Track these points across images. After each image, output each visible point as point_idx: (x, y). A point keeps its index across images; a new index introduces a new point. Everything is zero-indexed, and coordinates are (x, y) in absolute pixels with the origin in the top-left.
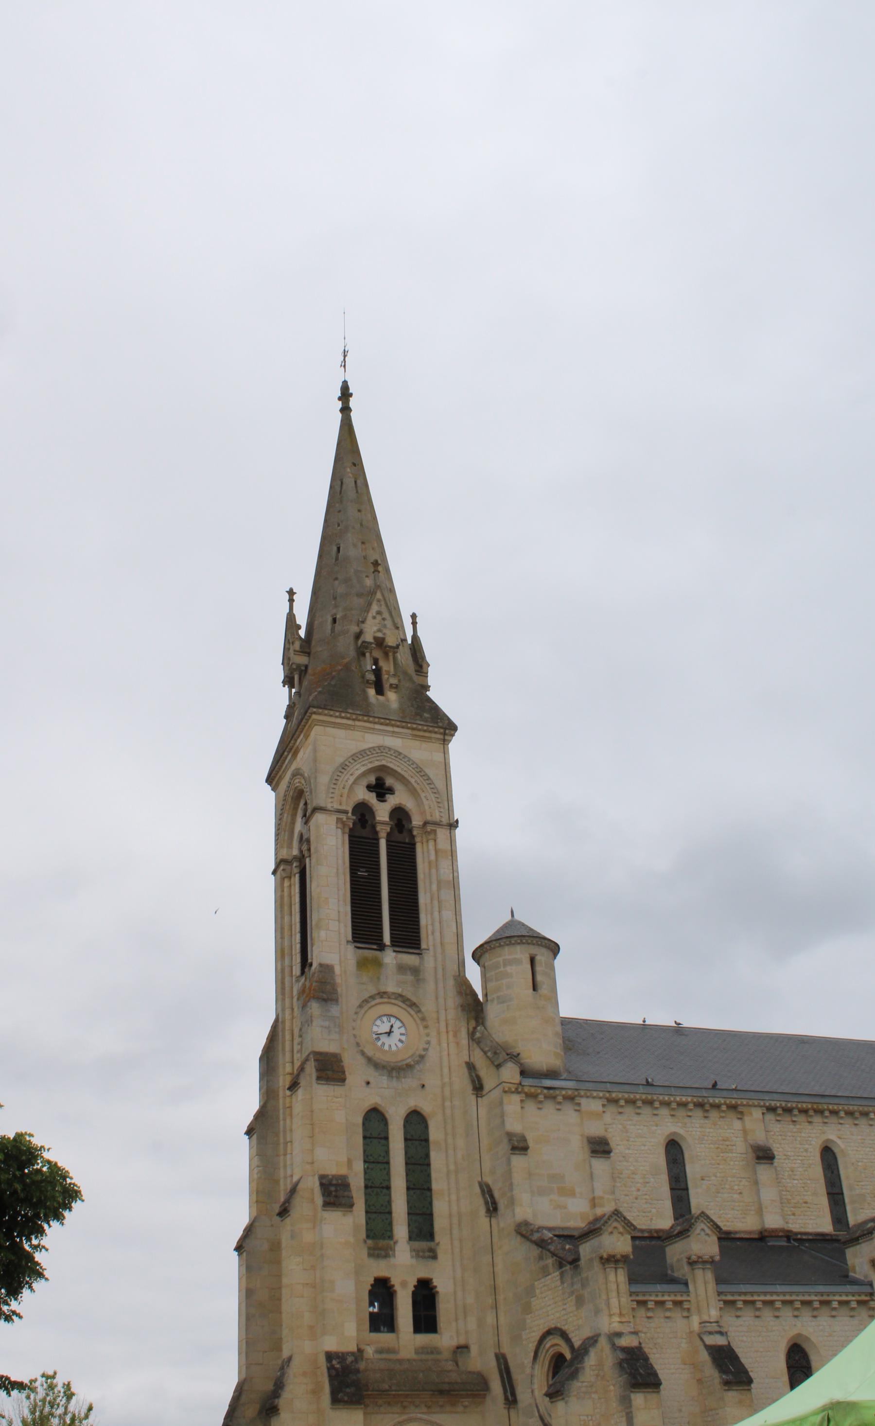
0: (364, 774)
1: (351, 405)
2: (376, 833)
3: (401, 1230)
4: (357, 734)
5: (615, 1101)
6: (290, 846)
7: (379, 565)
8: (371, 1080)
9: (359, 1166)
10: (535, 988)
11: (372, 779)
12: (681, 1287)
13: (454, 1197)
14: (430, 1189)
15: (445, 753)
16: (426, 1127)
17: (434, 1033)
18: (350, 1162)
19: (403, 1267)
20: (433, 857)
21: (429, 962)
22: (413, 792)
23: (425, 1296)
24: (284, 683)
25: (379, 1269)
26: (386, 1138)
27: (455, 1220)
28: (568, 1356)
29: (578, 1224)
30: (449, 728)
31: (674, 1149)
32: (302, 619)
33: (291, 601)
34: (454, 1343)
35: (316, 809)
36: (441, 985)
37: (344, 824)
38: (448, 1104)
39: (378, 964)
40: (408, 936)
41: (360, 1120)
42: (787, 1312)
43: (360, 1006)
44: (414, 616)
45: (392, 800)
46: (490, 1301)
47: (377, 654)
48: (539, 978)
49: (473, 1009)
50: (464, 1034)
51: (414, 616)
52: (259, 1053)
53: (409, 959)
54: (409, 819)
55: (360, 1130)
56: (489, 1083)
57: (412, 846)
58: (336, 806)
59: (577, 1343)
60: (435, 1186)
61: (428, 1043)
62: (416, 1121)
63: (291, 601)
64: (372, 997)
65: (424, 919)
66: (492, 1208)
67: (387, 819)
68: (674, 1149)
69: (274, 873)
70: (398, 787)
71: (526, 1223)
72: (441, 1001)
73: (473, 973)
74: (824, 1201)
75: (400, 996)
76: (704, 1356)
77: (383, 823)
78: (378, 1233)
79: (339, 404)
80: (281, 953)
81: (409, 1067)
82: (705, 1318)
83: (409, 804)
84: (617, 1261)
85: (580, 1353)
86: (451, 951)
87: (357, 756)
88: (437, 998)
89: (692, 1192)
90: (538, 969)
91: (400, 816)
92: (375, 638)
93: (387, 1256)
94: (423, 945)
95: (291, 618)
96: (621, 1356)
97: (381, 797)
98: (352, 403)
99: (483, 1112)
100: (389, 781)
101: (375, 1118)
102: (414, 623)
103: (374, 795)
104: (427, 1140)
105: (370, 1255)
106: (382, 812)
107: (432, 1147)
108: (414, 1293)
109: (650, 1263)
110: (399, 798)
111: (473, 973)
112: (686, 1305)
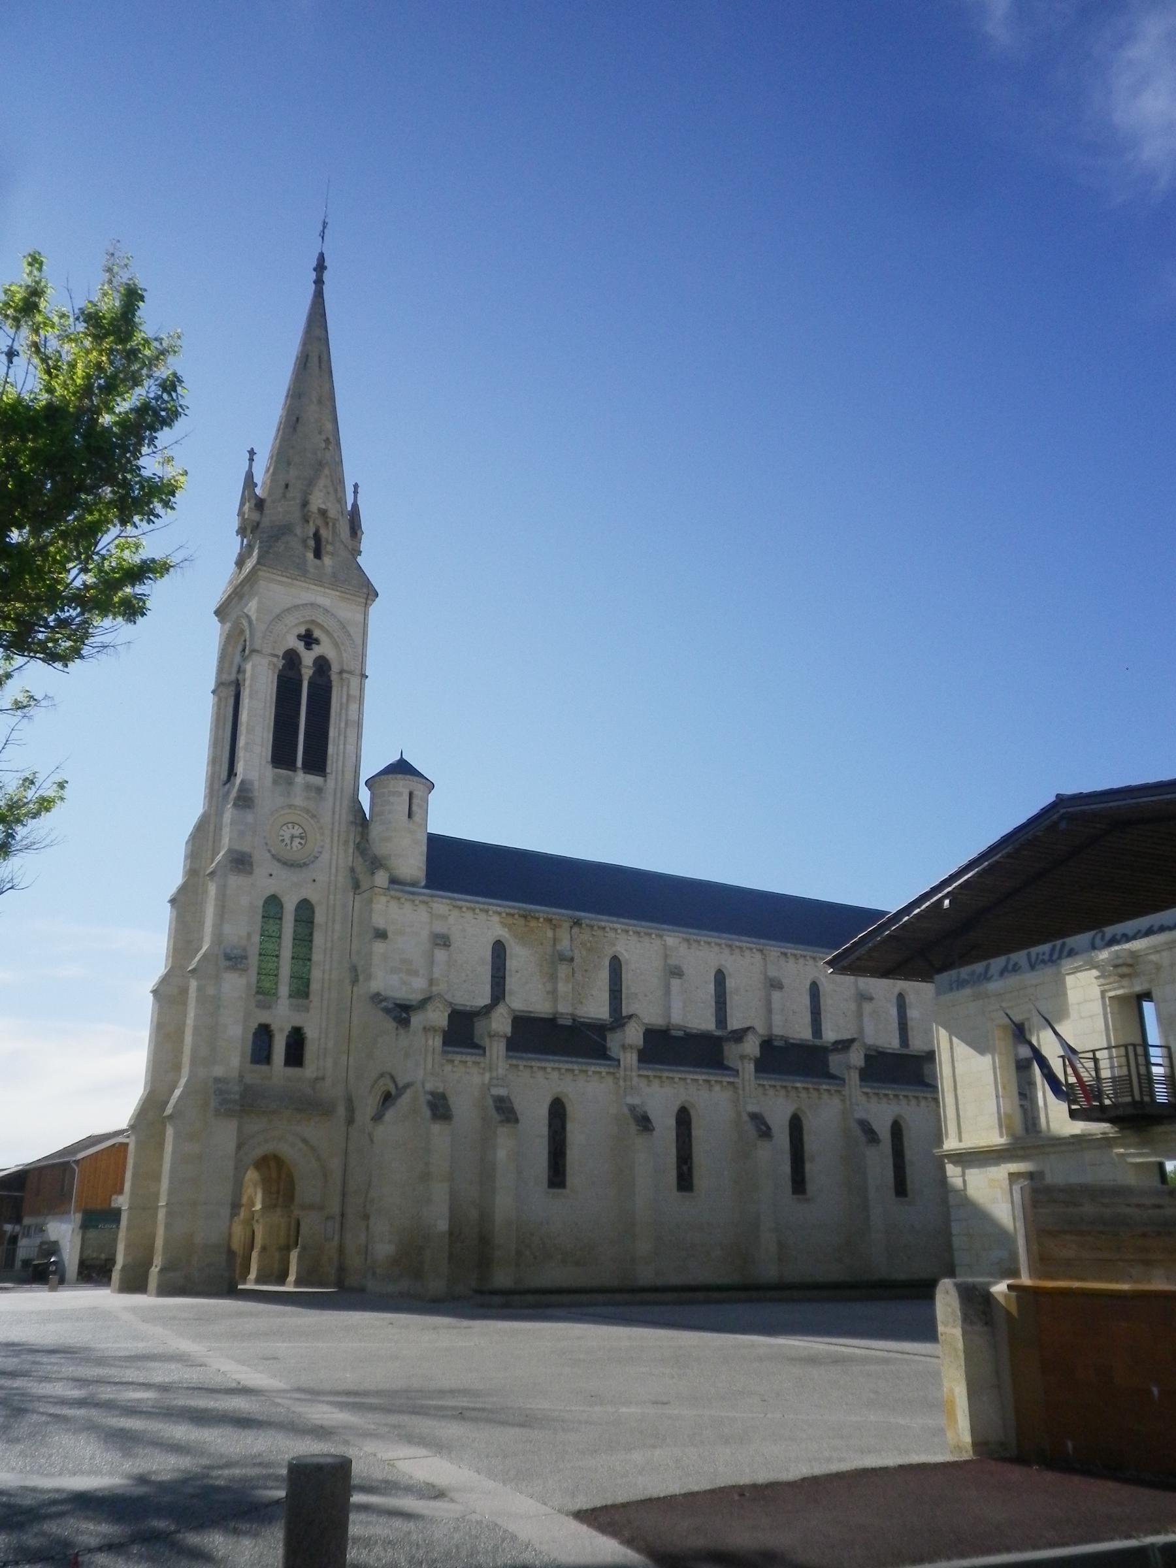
1: (325, 278)
2: (300, 675)
3: (284, 990)
7: (333, 441)
8: (274, 873)
9: (256, 938)
10: (410, 816)
11: (302, 631)
12: (481, 1052)
13: (327, 967)
15: (366, 614)
16: (313, 912)
17: (328, 841)
18: (249, 935)
20: (344, 700)
21: (331, 783)
22: (336, 645)
24: (238, 533)
25: (264, 1017)
27: (326, 985)
28: (393, 1092)
29: (415, 997)
30: (370, 594)
33: (251, 460)
34: (315, 1075)
35: (253, 651)
36: (338, 803)
37: (275, 665)
38: (332, 897)
39: (290, 783)
40: (317, 763)
41: (261, 903)
44: (356, 486)
45: (317, 650)
47: (319, 522)
48: (414, 808)
49: (361, 822)
51: (356, 486)
52: (190, 829)
53: (316, 780)
54: (329, 668)
55: (260, 911)
56: (365, 885)
61: (322, 847)
62: (305, 910)
63: (251, 460)
66: (355, 981)
67: (311, 664)
68: (499, 951)
69: (213, 692)
71: (378, 994)
72: (337, 817)
73: (365, 797)
74: (607, 995)
76: (490, 1102)
77: (307, 667)
78: (264, 994)
79: (313, 275)
80: (214, 761)
81: (305, 864)
82: (494, 1074)
84: (435, 1031)
85: (401, 1091)
86: (349, 776)
88: (334, 813)
89: (508, 980)
90: (415, 801)
91: (322, 665)
92: (319, 509)
93: (269, 1007)
94: (328, 770)
95: (249, 476)
96: (429, 1097)
98: (327, 276)
100: (317, 633)
101: (273, 905)
102: (356, 492)
103: (302, 643)
104: (312, 923)
105: (257, 1006)
106: (308, 658)
108: (288, 1037)
109: (462, 1031)
110: (325, 648)
111: (365, 797)
112: (483, 1065)
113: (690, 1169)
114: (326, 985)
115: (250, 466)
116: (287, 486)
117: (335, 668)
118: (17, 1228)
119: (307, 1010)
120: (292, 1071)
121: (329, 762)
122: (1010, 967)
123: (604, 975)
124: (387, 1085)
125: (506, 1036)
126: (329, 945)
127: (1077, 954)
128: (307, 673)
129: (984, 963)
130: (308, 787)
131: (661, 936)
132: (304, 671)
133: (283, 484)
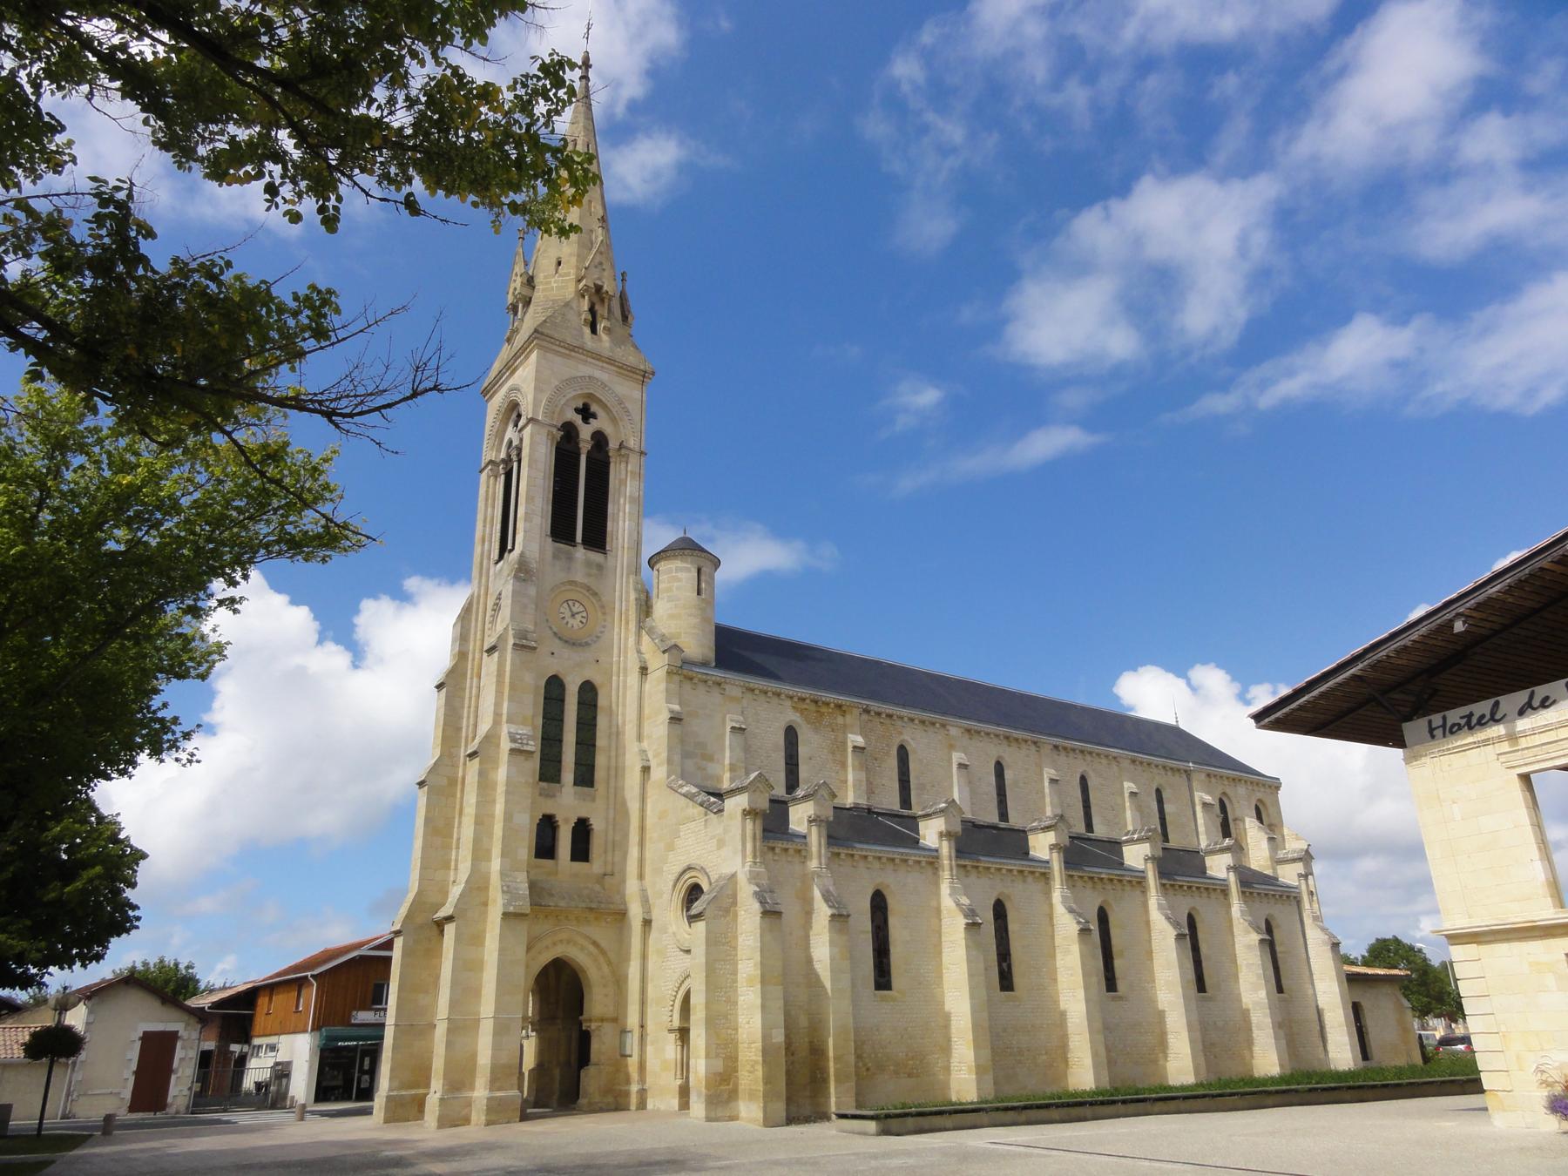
0: (574, 398)
3: (568, 775)
6: (499, 451)
19: (568, 804)
22: (614, 420)
23: (582, 831)
26: (563, 701)
31: (791, 735)
34: (602, 871)
39: (570, 558)
45: (595, 425)
53: (595, 556)
62: (589, 692)
68: (791, 735)
74: (897, 785)
83: (608, 430)
87: (569, 381)
91: (600, 439)
97: (586, 420)
100: (594, 408)
104: (595, 706)
106: (585, 432)
110: (601, 423)
113: (1009, 966)
114: (613, 773)
118: (246, 1048)
119: (593, 800)
120: (579, 866)
122: (1536, 703)
123: (893, 762)
127: (1554, 702)
128: (585, 444)
129: (1491, 702)
130: (588, 564)
131: (943, 726)
132: (581, 445)
133: (554, 262)
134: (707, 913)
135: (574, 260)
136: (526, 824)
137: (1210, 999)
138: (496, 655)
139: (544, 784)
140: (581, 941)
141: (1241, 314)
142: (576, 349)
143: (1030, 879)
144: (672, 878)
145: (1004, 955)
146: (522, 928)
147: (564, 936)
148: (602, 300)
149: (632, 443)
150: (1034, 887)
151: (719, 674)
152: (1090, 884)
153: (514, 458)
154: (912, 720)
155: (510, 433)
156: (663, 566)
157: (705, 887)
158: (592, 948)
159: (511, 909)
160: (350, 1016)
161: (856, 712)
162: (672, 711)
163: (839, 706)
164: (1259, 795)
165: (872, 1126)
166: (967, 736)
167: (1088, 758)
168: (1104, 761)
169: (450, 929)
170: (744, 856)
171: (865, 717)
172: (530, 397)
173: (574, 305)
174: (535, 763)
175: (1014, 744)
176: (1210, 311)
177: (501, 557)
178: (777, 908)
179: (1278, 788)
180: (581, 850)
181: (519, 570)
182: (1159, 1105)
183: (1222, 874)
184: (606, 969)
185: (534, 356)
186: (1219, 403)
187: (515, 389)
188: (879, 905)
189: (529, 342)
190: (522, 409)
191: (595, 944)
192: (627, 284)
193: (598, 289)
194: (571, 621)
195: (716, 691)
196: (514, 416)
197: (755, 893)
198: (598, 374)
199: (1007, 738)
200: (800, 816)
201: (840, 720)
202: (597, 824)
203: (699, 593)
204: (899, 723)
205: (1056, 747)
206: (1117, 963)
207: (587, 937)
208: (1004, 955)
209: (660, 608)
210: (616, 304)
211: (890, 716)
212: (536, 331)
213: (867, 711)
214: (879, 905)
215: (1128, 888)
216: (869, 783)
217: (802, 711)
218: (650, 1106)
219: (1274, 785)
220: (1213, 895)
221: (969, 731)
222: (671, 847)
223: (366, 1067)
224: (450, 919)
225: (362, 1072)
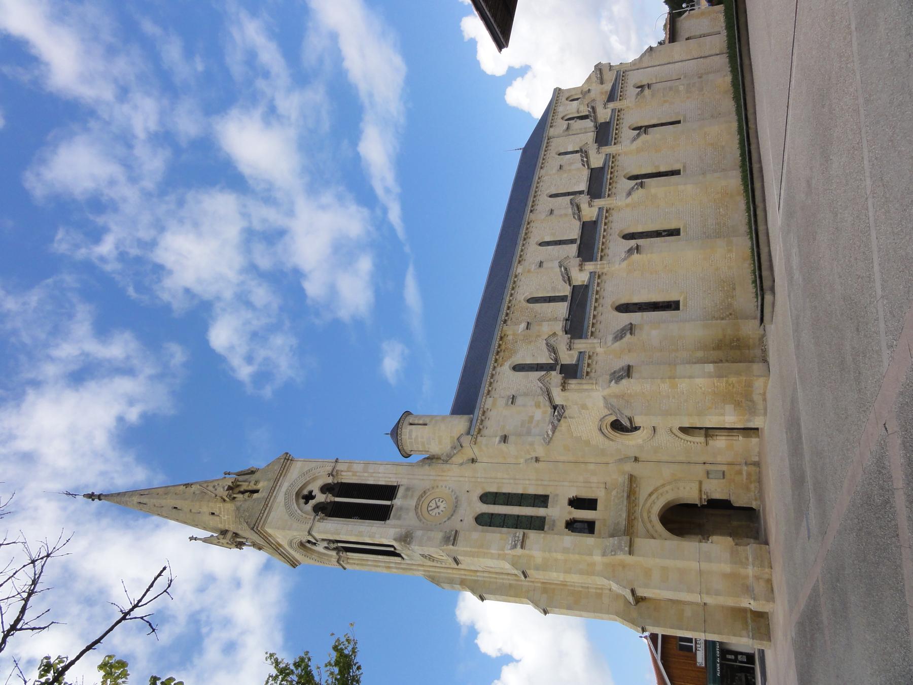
0: (298, 504)
2: (331, 502)
3: (540, 512)
4: (275, 505)
5: (489, 391)
6: (331, 556)
11: (302, 501)
13: (527, 482)
14: (522, 494)
16: (489, 493)
19: (559, 512)
22: (314, 479)
26: (492, 514)
27: (539, 483)
31: (518, 368)
32: (208, 534)
33: (196, 539)
34: (603, 490)
39: (401, 508)
42: (600, 309)
43: (420, 520)
45: (317, 492)
46: (583, 465)
48: (421, 422)
50: (444, 466)
53: (400, 493)
57: (343, 484)
58: (311, 521)
59: (606, 412)
60: (520, 491)
63: (196, 539)
64: (417, 513)
65: (382, 482)
68: (518, 368)
70: (309, 488)
74: (552, 304)
75: (419, 499)
81: (457, 502)
83: (320, 483)
87: (287, 506)
90: (416, 422)
91: (325, 489)
97: (313, 497)
99: (485, 459)
100: (305, 492)
106: (321, 498)
107: (500, 491)
110: (315, 488)
113: (664, 231)
114: (539, 483)
115: (200, 539)
116: (213, 514)
117: (330, 480)
119: (557, 495)
120: (600, 505)
121: (390, 484)
123: (537, 306)
124: (608, 430)
125: (571, 338)
126: (512, 481)
128: (331, 498)
130: (405, 497)
131: (516, 276)
133: (212, 517)
134: (629, 415)
135: (211, 504)
136: (570, 539)
137: (685, 118)
138: (459, 557)
139: (546, 527)
140: (648, 504)
141: (353, 208)
142: (267, 504)
143: (610, 219)
144: (607, 442)
145: (658, 234)
146: (640, 542)
147: (645, 515)
148: (239, 486)
149: (329, 469)
150: (615, 217)
151: (478, 412)
152: (614, 185)
153: (335, 545)
154: (512, 295)
155: (320, 548)
156: (408, 448)
157: (613, 418)
158: (654, 497)
159: (627, 549)
160: (700, 668)
161: (505, 327)
162: (500, 442)
163: (501, 338)
164: (564, 99)
165: (768, 298)
166: (523, 262)
167: (539, 193)
168: (541, 184)
169: (641, 592)
170: (592, 389)
171: (509, 322)
172: (295, 533)
173: (238, 504)
174: (532, 535)
175: (529, 235)
176: (352, 222)
177: (399, 555)
178: (626, 368)
179: (560, 89)
180: (591, 504)
181: (405, 541)
182: (751, 125)
183: (609, 111)
184: (667, 488)
185: (269, 531)
186: (395, 214)
187: (290, 544)
188: (624, 308)
189: (259, 533)
190: (304, 540)
191: (650, 495)
192: (232, 471)
193: (230, 488)
194: (441, 508)
195: (488, 414)
196: (309, 545)
197: (617, 382)
198: (284, 489)
199: (525, 239)
200: (568, 357)
201: (510, 338)
202: (573, 493)
203: (425, 425)
204: (513, 302)
205: (531, 211)
206: (663, 169)
207: (646, 500)
208: (658, 234)
209: (435, 449)
210: (241, 478)
211: (509, 308)
212: (252, 529)
213: (505, 322)
214: (624, 308)
215: (617, 163)
216: (550, 320)
217: (504, 360)
218: (756, 459)
219: (558, 92)
220: (622, 116)
221: (520, 262)
222: (587, 443)
223: (733, 657)
224: (633, 592)
225: (736, 660)
